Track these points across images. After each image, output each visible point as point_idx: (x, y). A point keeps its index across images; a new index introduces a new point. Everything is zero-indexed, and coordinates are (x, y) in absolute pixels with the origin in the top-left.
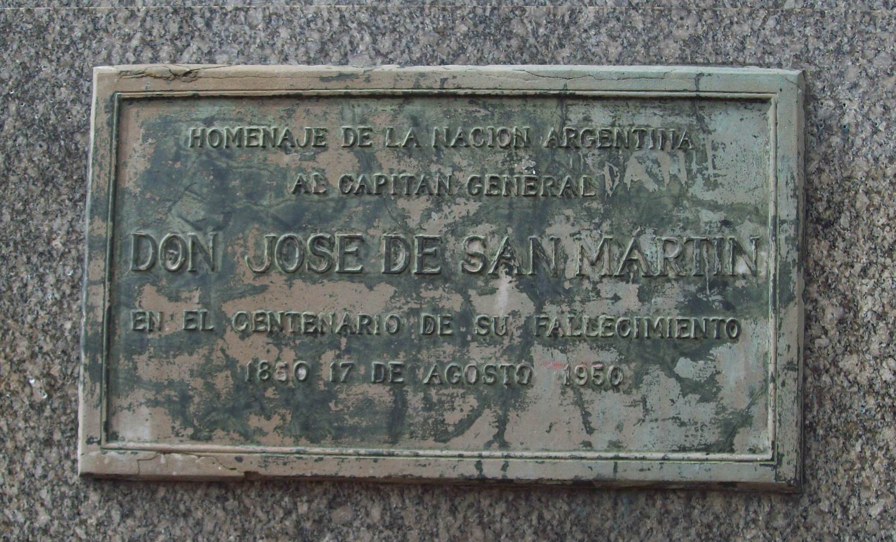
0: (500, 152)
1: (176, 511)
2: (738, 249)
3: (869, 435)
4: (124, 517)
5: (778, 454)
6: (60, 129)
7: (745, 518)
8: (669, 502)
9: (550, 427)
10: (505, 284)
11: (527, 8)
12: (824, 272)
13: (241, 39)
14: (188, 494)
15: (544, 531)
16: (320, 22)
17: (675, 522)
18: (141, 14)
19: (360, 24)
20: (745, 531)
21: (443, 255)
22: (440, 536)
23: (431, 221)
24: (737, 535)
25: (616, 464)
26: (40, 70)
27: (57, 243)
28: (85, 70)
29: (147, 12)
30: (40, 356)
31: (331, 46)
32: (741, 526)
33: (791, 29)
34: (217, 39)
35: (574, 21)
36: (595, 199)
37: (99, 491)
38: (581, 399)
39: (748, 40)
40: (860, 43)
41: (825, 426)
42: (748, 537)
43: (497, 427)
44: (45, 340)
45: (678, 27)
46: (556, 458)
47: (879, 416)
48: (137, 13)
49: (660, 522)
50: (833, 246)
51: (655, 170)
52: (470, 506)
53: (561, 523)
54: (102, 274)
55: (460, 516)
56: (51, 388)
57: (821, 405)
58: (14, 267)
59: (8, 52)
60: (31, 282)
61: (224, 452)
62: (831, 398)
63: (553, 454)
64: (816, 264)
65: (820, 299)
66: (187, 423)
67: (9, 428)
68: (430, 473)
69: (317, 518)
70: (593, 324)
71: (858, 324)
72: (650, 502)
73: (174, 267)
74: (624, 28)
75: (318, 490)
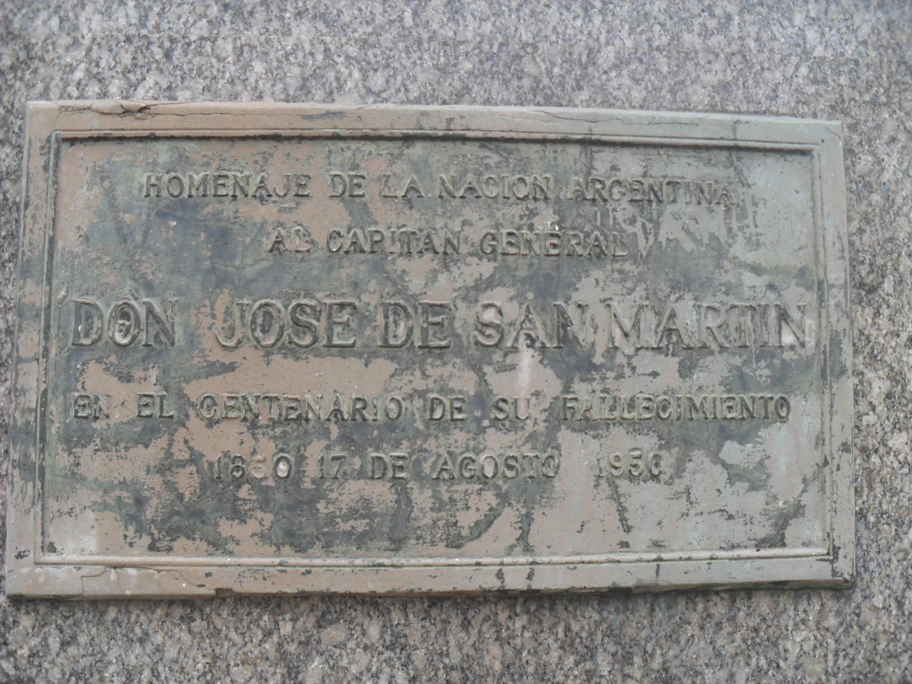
0: (517, 204)
1: (131, 635)
2: (783, 316)
4: (64, 644)
5: (834, 547)
7: (794, 620)
9: (582, 526)
10: (527, 358)
11: (540, 45)
12: (870, 342)
13: (208, 73)
14: (145, 614)
15: (572, 645)
16: (300, 55)
17: (719, 626)
18: (86, 42)
19: (348, 57)
20: (794, 633)
21: (451, 325)
22: (451, 655)
23: (436, 284)
24: (786, 638)
25: (658, 566)
28: (17, 106)
29: (94, 39)
31: (314, 83)
32: (790, 628)
33: (824, 78)
34: (178, 73)
36: (627, 260)
37: (33, 614)
38: (617, 492)
39: (780, 88)
40: (897, 94)
41: (876, 512)
42: (798, 640)
43: (520, 528)
45: (706, 72)
46: (590, 562)
48: (81, 40)
49: (702, 628)
50: (877, 314)
51: (693, 227)
52: (486, 619)
53: (591, 634)
55: (474, 632)
57: (871, 488)
61: (189, 565)
62: (881, 481)
63: (586, 558)
64: (861, 333)
65: (866, 371)
66: (141, 530)
68: (440, 586)
69: (303, 639)
70: (631, 405)
71: (906, 398)
72: (690, 606)
74: (647, 71)
75: (304, 606)
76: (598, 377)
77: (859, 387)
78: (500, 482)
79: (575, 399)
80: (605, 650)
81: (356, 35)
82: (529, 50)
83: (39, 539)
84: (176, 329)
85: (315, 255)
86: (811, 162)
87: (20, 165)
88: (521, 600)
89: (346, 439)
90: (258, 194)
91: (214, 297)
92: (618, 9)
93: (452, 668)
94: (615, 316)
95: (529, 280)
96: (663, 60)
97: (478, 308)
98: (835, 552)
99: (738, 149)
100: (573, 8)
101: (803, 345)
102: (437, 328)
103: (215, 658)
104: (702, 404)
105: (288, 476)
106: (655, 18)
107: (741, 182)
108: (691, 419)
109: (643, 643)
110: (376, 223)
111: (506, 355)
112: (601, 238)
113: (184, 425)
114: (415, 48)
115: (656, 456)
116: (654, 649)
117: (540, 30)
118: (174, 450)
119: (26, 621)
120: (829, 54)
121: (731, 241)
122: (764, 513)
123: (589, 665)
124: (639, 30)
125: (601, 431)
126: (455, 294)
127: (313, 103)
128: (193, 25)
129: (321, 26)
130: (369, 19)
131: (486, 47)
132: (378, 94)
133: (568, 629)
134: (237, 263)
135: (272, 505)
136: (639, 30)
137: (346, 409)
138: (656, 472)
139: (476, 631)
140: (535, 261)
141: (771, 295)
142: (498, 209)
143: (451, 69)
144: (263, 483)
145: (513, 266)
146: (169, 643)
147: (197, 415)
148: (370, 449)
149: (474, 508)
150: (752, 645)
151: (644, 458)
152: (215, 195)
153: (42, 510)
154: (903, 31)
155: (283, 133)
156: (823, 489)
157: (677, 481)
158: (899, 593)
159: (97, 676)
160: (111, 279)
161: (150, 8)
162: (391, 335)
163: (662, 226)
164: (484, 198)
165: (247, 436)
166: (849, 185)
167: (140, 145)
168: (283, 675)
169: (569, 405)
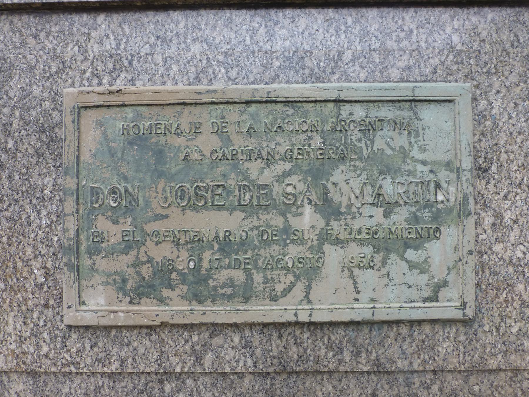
1: (123, 343)
2: (438, 186)
3: (510, 288)
4: (92, 347)
5: (464, 302)
6: (46, 126)
7: (443, 336)
8: (400, 328)
10: (308, 210)
13: (150, 72)
15: (331, 347)
16: (195, 61)
17: (404, 339)
18: (91, 58)
19: (218, 62)
20: (443, 343)
21: (271, 194)
22: (273, 351)
23: (263, 174)
24: (439, 345)
25: (374, 311)
26: (33, 91)
27: (47, 192)
28: (59, 91)
29: (95, 57)
30: (40, 256)
31: (202, 75)
32: (441, 341)
33: (462, 61)
34: (136, 72)
35: (340, 58)
36: (358, 160)
38: (352, 274)
39: (438, 67)
40: (501, 68)
41: (486, 283)
42: (445, 346)
43: (305, 292)
44: (42, 247)
46: (339, 309)
47: (515, 277)
48: (88, 57)
49: (396, 340)
50: (488, 183)
51: (391, 142)
53: (341, 342)
54: (72, 210)
55: (284, 340)
56: (47, 275)
57: (483, 272)
58: (22, 206)
59: (13, 81)
60: (32, 214)
63: (338, 307)
64: (479, 193)
65: (481, 212)
66: (125, 295)
67: (23, 299)
68: (266, 320)
69: (203, 343)
70: (360, 232)
71: (502, 226)
72: (390, 329)
73: (115, 205)
76: (343, 218)
77: (477, 221)
78: (295, 270)
79: (332, 229)
80: (348, 349)
81: (223, 50)
82: (308, 54)
83: (77, 299)
84: (139, 199)
85: (204, 162)
86: (454, 106)
87: (62, 120)
88: (306, 325)
89: (221, 250)
90: (176, 132)
91: (157, 183)
92: (353, 30)
93: (274, 358)
94: (351, 188)
95: (309, 171)
96: (377, 56)
97: (284, 186)
98: (464, 304)
99: (415, 101)
100: (330, 31)
101: (448, 200)
102: (264, 196)
103: (162, 353)
104: (395, 230)
105: (194, 268)
106: (373, 34)
107: (417, 118)
108: (390, 238)
109: (366, 346)
110: (234, 145)
111: (297, 208)
112: (345, 150)
113: (144, 245)
114: (251, 56)
115: (372, 257)
116: (372, 350)
117: (314, 43)
118: (140, 256)
119: (74, 336)
120: (464, 48)
121: (411, 149)
122: (427, 285)
123: (340, 357)
124: (364, 40)
125: (344, 245)
126: (273, 179)
127: (202, 86)
128: (142, 47)
129: (205, 46)
130: (228, 41)
131: (286, 54)
132: (234, 80)
133: (329, 339)
134: (167, 166)
135: (187, 282)
136: (364, 40)
137: (221, 235)
138: (372, 264)
139: (285, 339)
140: (312, 162)
141: (432, 176)
142: (293, 137)
143: (269, 66)
144: (183, 272)
145: (301, 165)
146: (140, 346)
147: (151, 240)
148: (233, 255)
149: (283, 282)
150: (421, 349)
151: (366, 258)
152: (155, 133)
153: (79, 286)
154: (504, 33)
155: (187, 101)
156: (458, 273)
157: (382, 269)
158: (497, 324)
159: (107, 362)
160: (107, 175)
161: (122, 39)
162: (242, 199)
163: (375, 143)
164: (286, 131)
165: (175, 249)
166: (474, 117)
167: (118, 109)
168: (194, 361)
169: (329, 232)
